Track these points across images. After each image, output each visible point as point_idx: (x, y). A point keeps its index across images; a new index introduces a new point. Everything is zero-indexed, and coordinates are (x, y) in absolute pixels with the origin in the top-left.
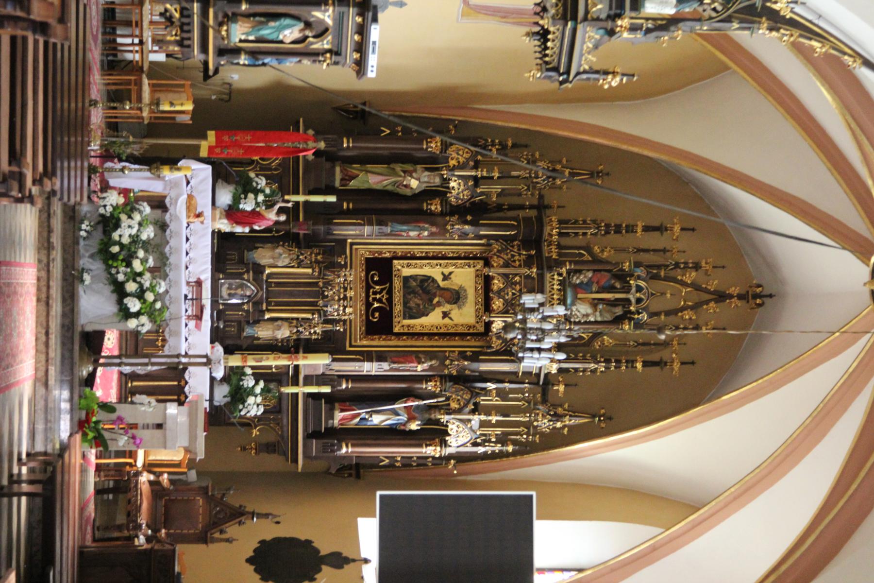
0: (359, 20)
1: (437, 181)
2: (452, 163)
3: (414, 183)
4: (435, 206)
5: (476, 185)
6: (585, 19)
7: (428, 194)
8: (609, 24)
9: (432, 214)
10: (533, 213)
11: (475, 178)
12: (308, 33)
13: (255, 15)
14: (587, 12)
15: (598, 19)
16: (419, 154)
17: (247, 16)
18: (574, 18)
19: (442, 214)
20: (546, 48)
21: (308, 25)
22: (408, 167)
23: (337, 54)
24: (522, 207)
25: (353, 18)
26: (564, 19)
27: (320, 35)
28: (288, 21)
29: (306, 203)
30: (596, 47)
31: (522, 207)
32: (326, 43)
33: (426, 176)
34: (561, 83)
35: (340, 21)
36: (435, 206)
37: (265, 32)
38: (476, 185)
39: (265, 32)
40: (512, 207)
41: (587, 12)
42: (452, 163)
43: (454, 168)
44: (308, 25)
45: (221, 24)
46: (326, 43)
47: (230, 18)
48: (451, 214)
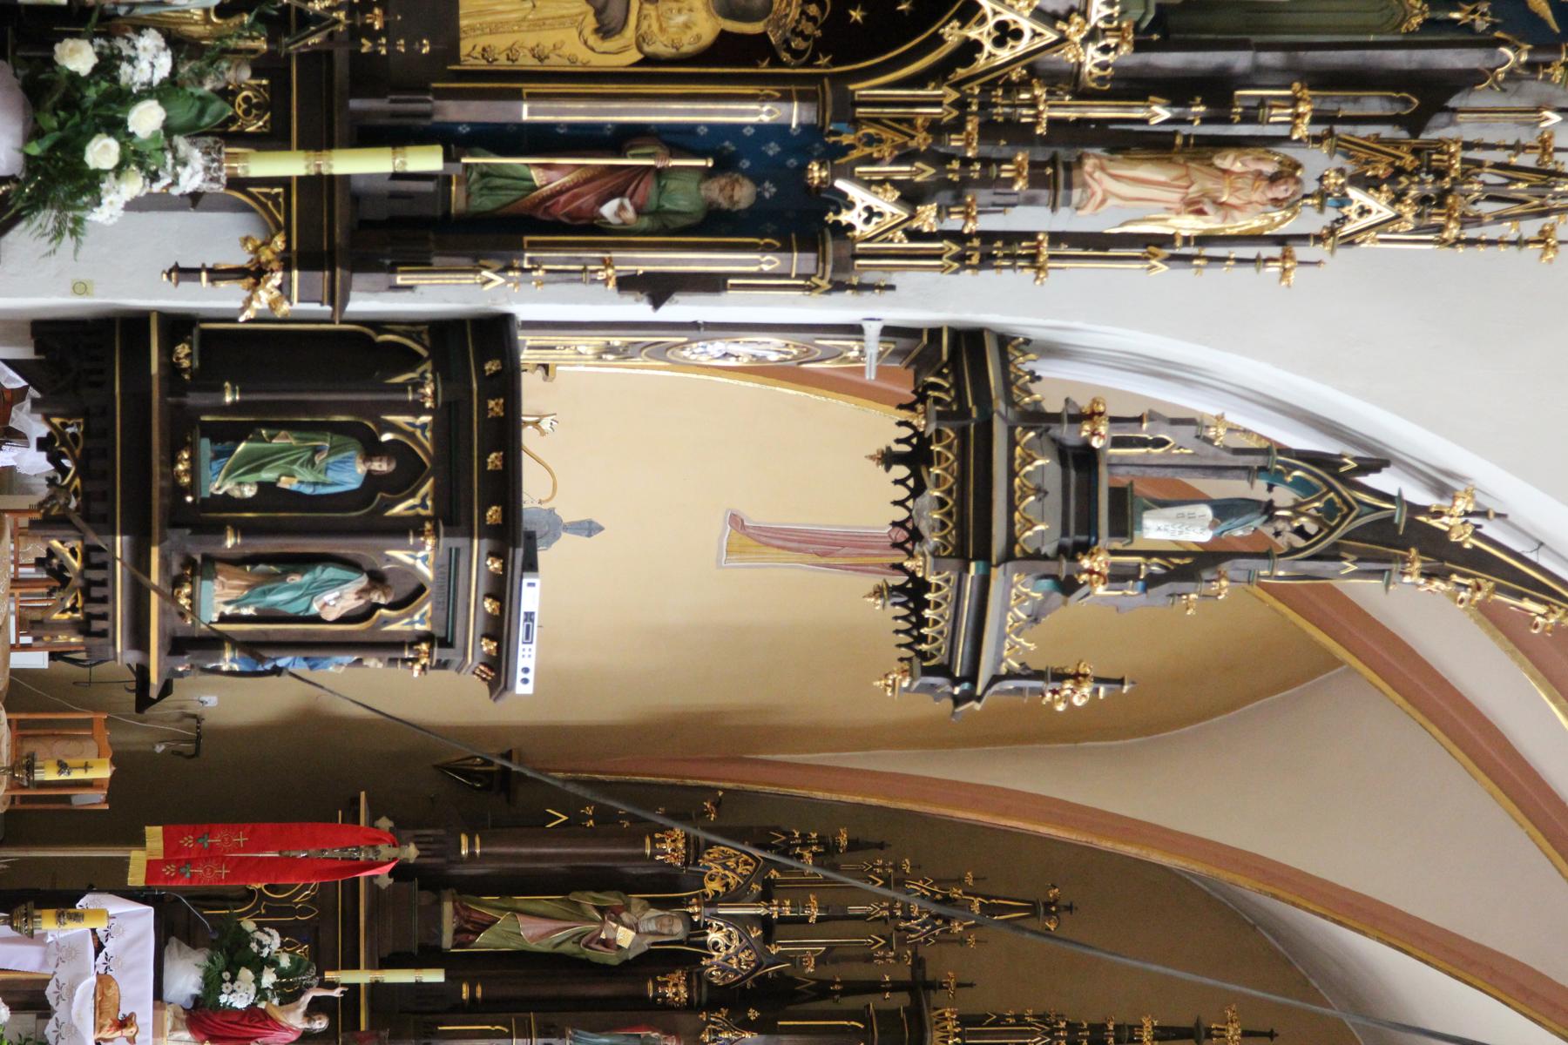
0: (495, 565)
1: (679, 929)
2: (712, 887)
3: (625, 937)
4: (675, 989)
5: (768, 938)
6: (1009, 556)
7: (658, 960)
8: (1063, 568)
9: (667, 1006)
10: (901, 1001)
11: (766, 923)
12: (377, 597)
13: (255, 560)
14: (1012, 539)
15: (1038, 556)
16: (634, 870)
17: (239, 561)
18: (984, 554)
19: (691, 1007)
20: (923, 622)
21: (377, 579)
22: (612, 899)
23: (446, 643)
24: (875, 987)
25: (479, 561)
26: (961, 556)
27: (403, 603)
28: (331, 572)
29: (375, 987)
30: (1035, 618)
31: (875, 987)
32: (418, 620)
33: (651, 920)
34: (958, 701)
35: (451, 569)
36: (675, 989)
37: (280, 598)
38: (768, 938)
39: (280, 598)
40: (852, 988)
41: (1012, 539)
42: (712, 887)
43: (717, 900)
44: (377, 579)
45: (177, 583)
46: (418, 620)
47: (201, 568)
48: (712, 1006)
